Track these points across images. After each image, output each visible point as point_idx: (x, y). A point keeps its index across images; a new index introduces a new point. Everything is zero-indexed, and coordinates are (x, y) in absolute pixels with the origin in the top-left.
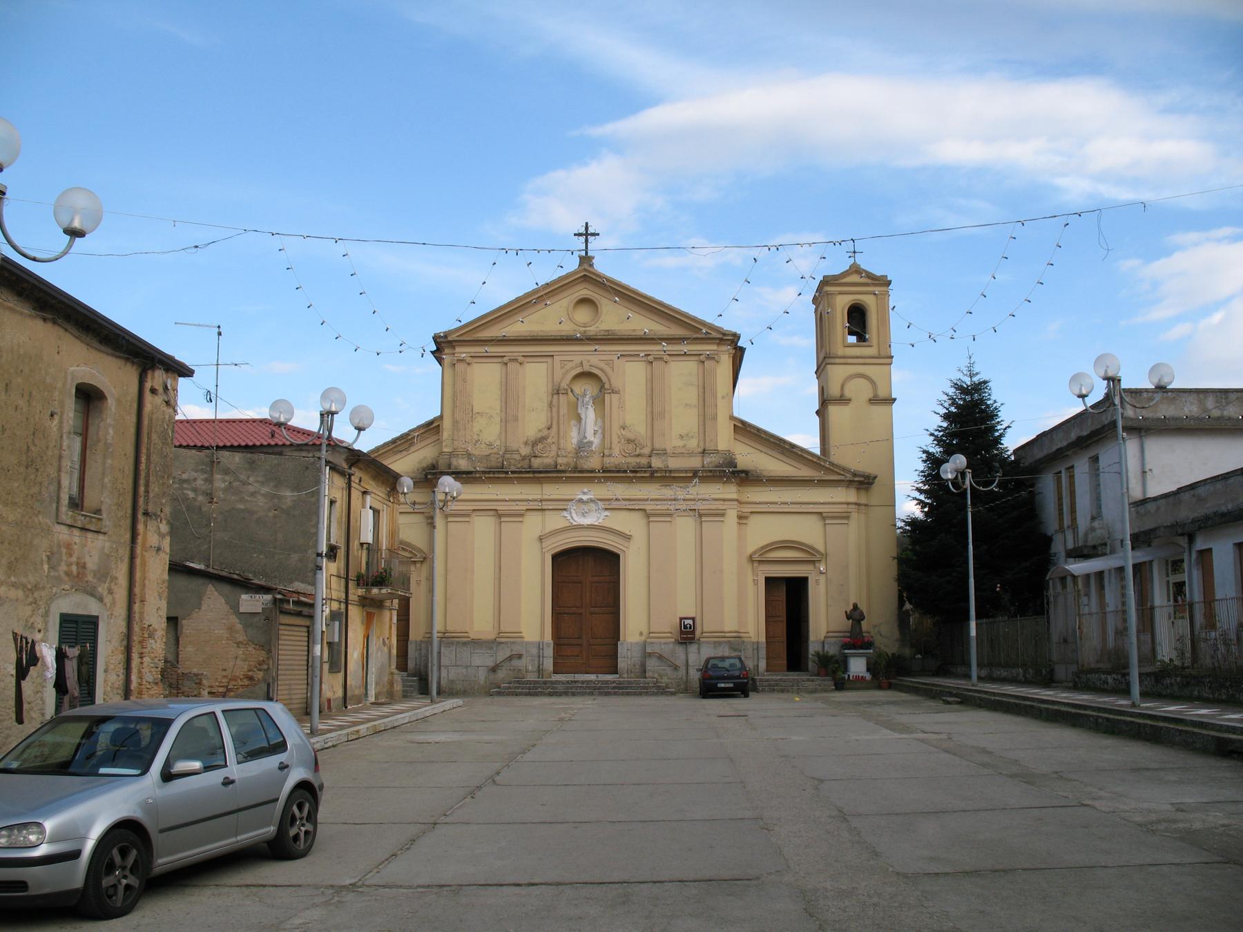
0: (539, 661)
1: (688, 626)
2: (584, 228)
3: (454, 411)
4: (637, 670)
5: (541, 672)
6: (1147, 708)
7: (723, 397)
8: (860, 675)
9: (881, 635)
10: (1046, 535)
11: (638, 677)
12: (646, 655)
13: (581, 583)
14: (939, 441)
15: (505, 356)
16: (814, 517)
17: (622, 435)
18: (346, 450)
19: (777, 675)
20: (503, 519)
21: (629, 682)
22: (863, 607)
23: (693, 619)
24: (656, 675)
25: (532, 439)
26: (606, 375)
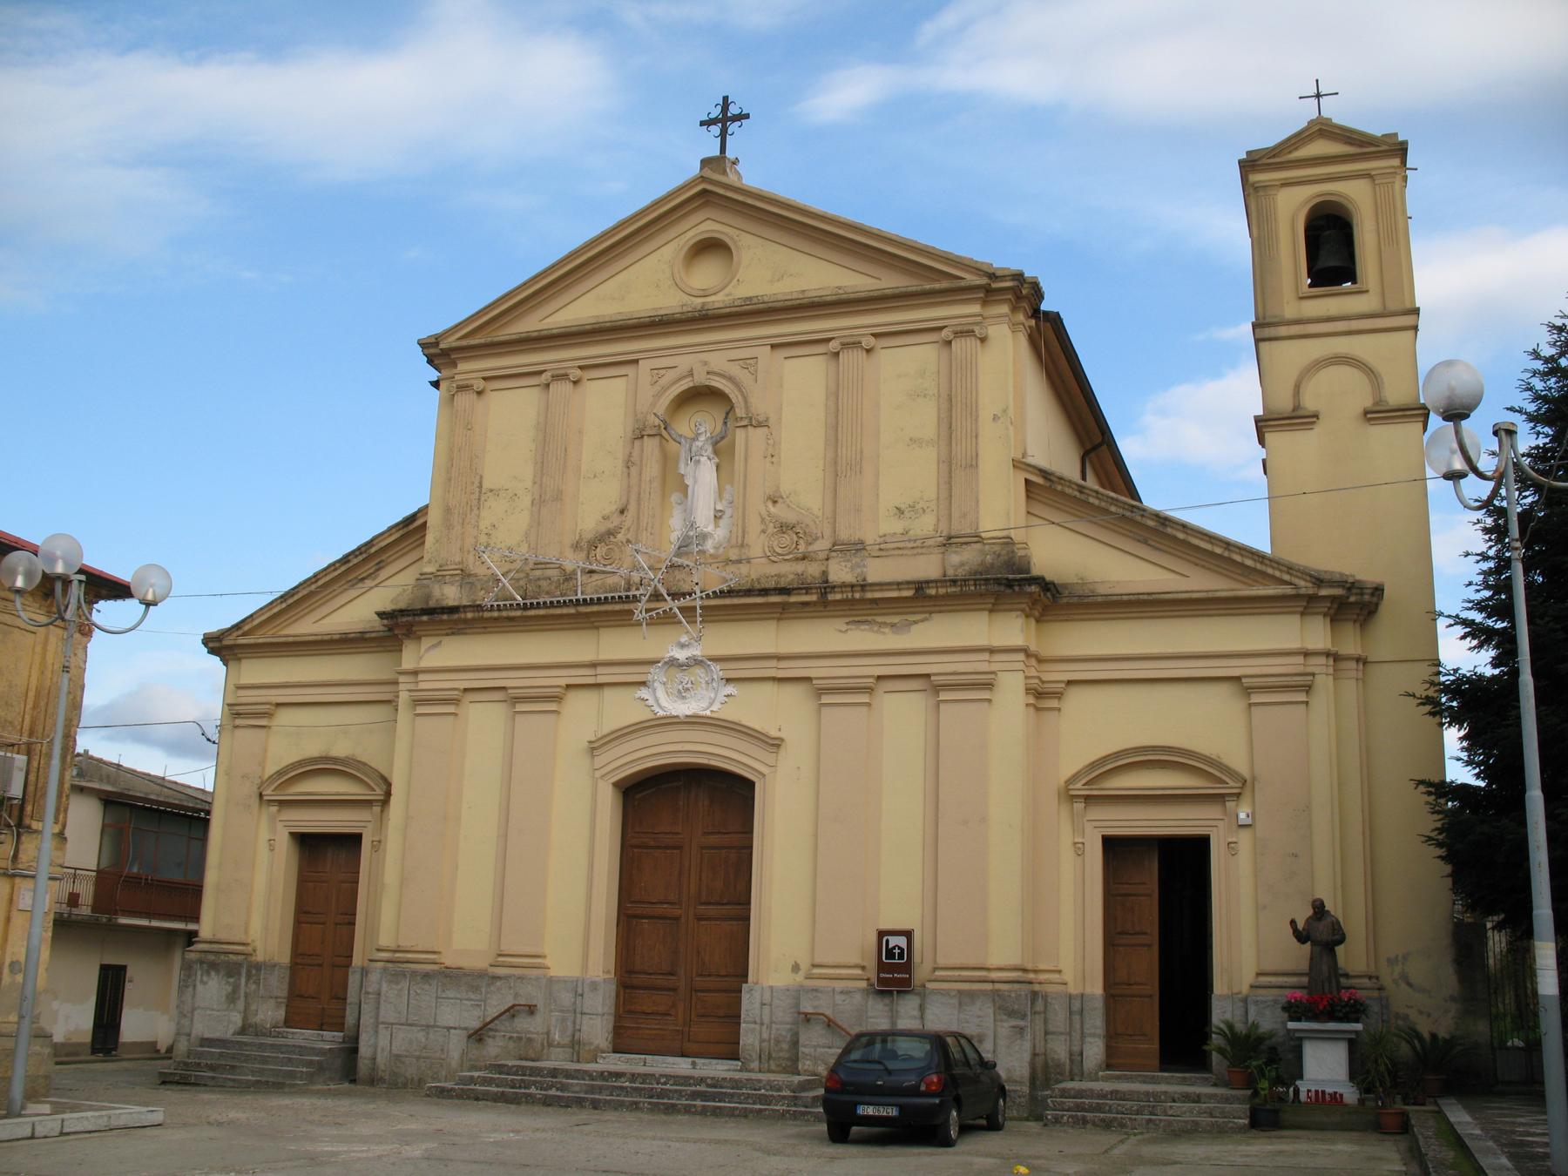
1: (897, 951)
7: (995, 418)
8: (1329, 1090)
9: (1410, 985)
13: (680, 848)
15: (545, 371)
16: (1223, 690)
23: (908, 934)
25: (589, 536)
26: (740, 390)
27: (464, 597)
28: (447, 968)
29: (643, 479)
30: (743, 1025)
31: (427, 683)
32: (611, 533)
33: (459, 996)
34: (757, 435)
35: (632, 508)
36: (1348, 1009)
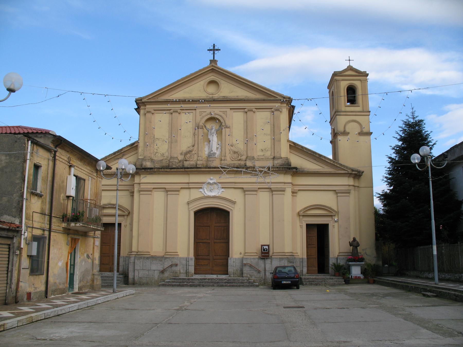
0: (187, 268)
1: (266, 249)
2: (213, 47)
3: (144, 137)
4: (238, 273)
5: (188, 273)
6: (441, 285)
8: (358, 276)
9: (367, 255)
10: (458, 200)
11: (239, 277)
12: (243, 265)
14: (397, 152)
15: (171, 110)
17: (231, 149)
18: (53, 136)
19: (312, 276)
20: (169, 193)
21: (234, 280)
22: (358, 239)
23: (268, 246)
24: (248, 276)
25: (185, 152)
26: (223, 119)
27: (152, 165)
28: (152, 256)
29: (199, 139)
30: (229, 267)
31: (143, 186)
32: (190, 151)
33: (156, 262)
34: (227, 130)
35: (196, 146)
36: (361, 260)
